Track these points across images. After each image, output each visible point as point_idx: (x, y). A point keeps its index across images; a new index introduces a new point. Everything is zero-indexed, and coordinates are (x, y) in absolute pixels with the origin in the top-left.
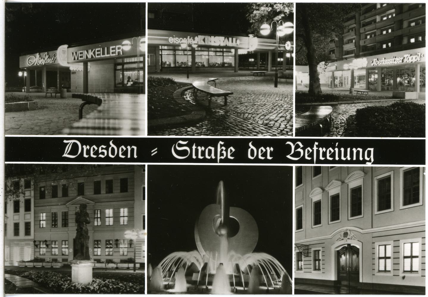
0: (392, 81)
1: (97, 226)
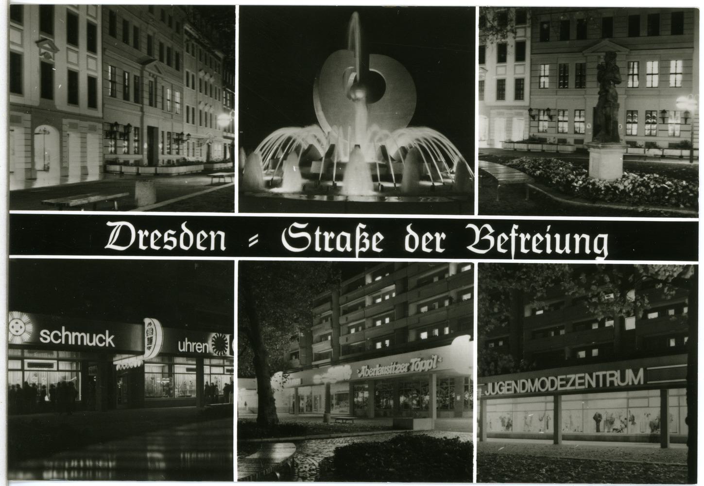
0: (392, 402)
1: (633, 87)
